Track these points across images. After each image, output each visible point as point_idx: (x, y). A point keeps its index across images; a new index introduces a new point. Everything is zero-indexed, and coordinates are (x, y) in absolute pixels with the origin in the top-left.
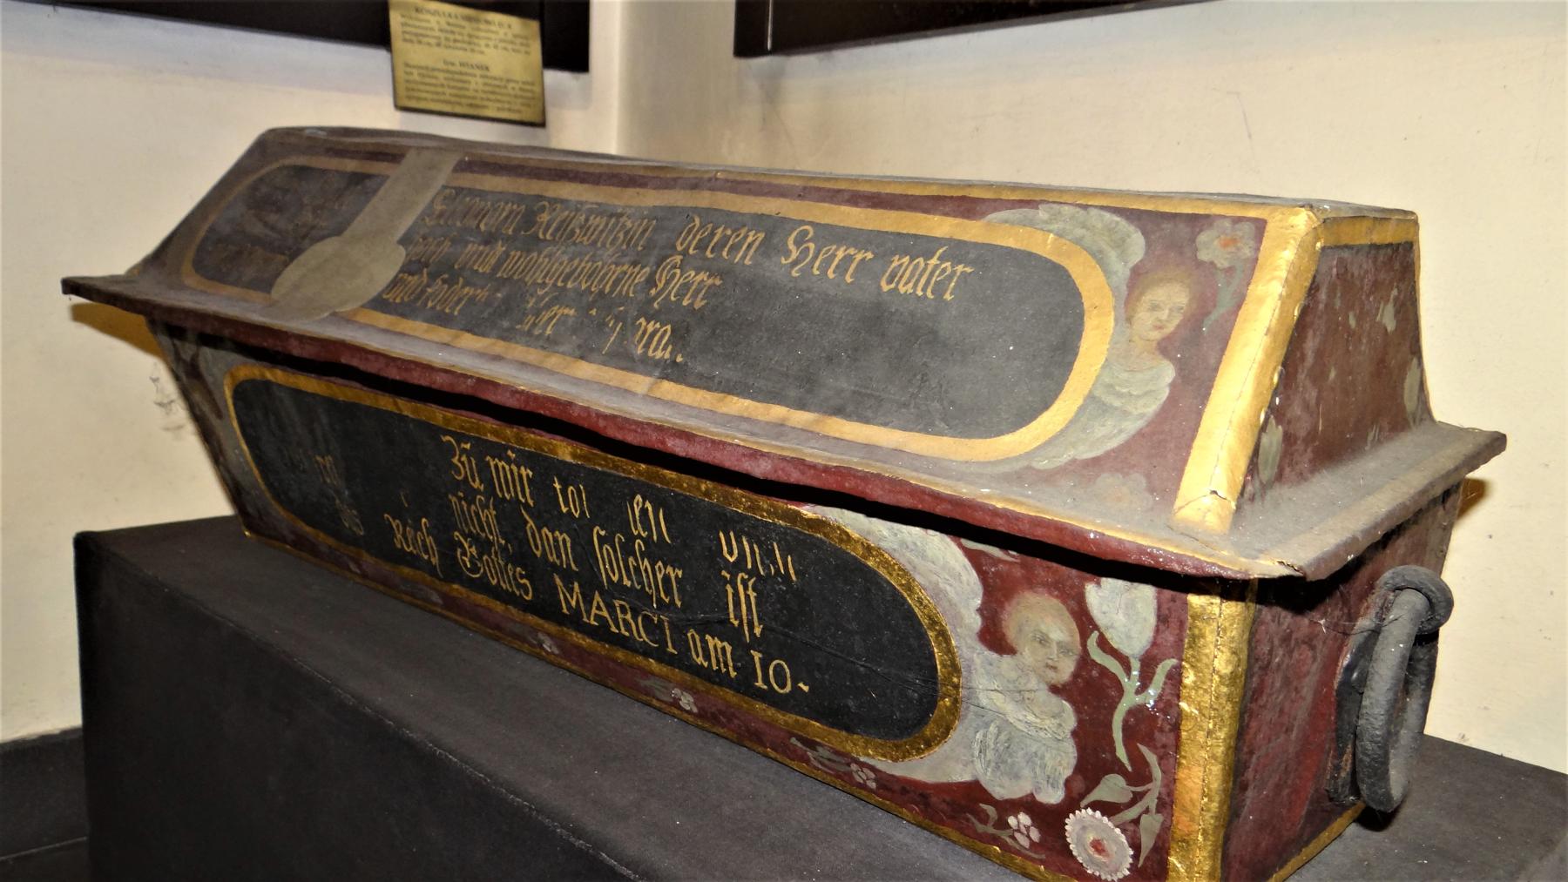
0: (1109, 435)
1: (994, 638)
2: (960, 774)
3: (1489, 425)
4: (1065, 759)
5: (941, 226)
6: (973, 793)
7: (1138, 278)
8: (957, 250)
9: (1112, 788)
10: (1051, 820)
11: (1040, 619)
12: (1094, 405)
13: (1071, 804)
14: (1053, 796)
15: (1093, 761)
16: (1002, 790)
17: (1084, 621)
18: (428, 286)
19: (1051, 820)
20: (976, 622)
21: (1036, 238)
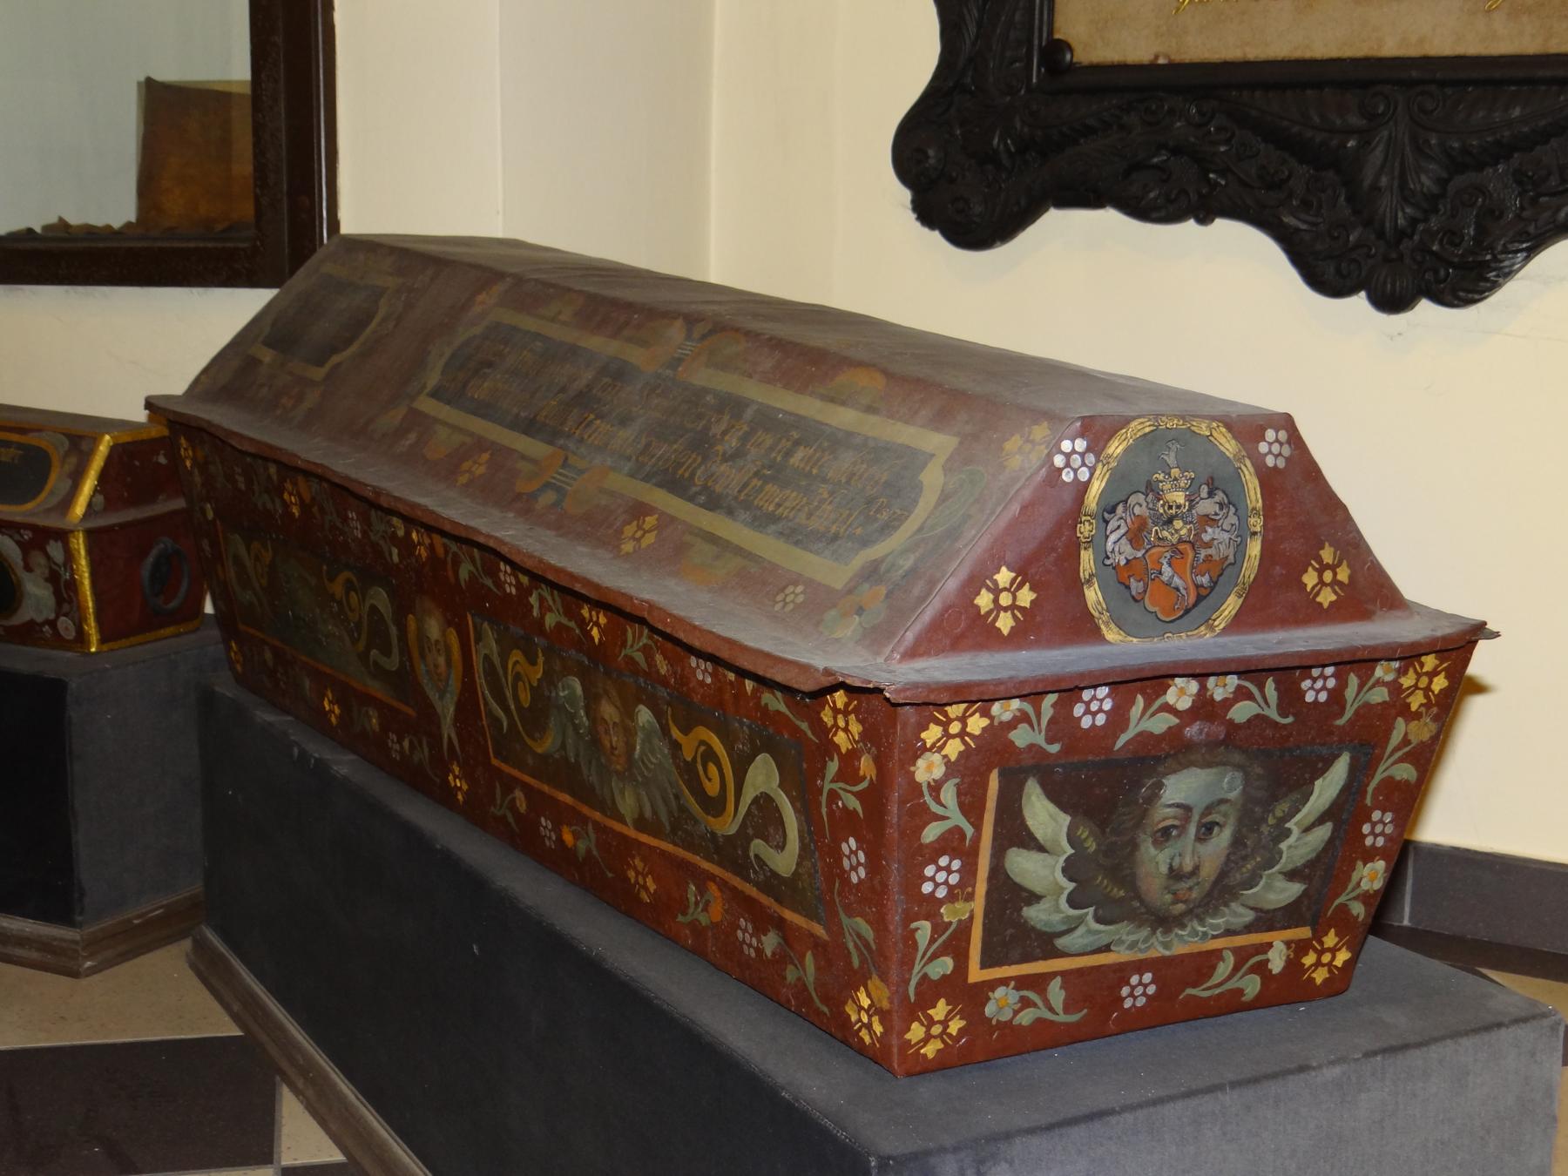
0: (54, 501)
1: (28, 568)
2: (27, 618)
3: (1474, 613)
4: (52, 602)
5: (15, 437)
6: (32, 623)
7: (67, 455)
8: (20, 446)
9: (66, 607)
10: (52, 624)
11: (38, 559)
12: (52, 493)
13: (57, 617)
14: (52, 616)
15: (60, 600)
16: (39, 619)
17: (48, 557)
18: (1174, 826)
19: (52, 624)
20: (21, 563)
21: (31, 439)
